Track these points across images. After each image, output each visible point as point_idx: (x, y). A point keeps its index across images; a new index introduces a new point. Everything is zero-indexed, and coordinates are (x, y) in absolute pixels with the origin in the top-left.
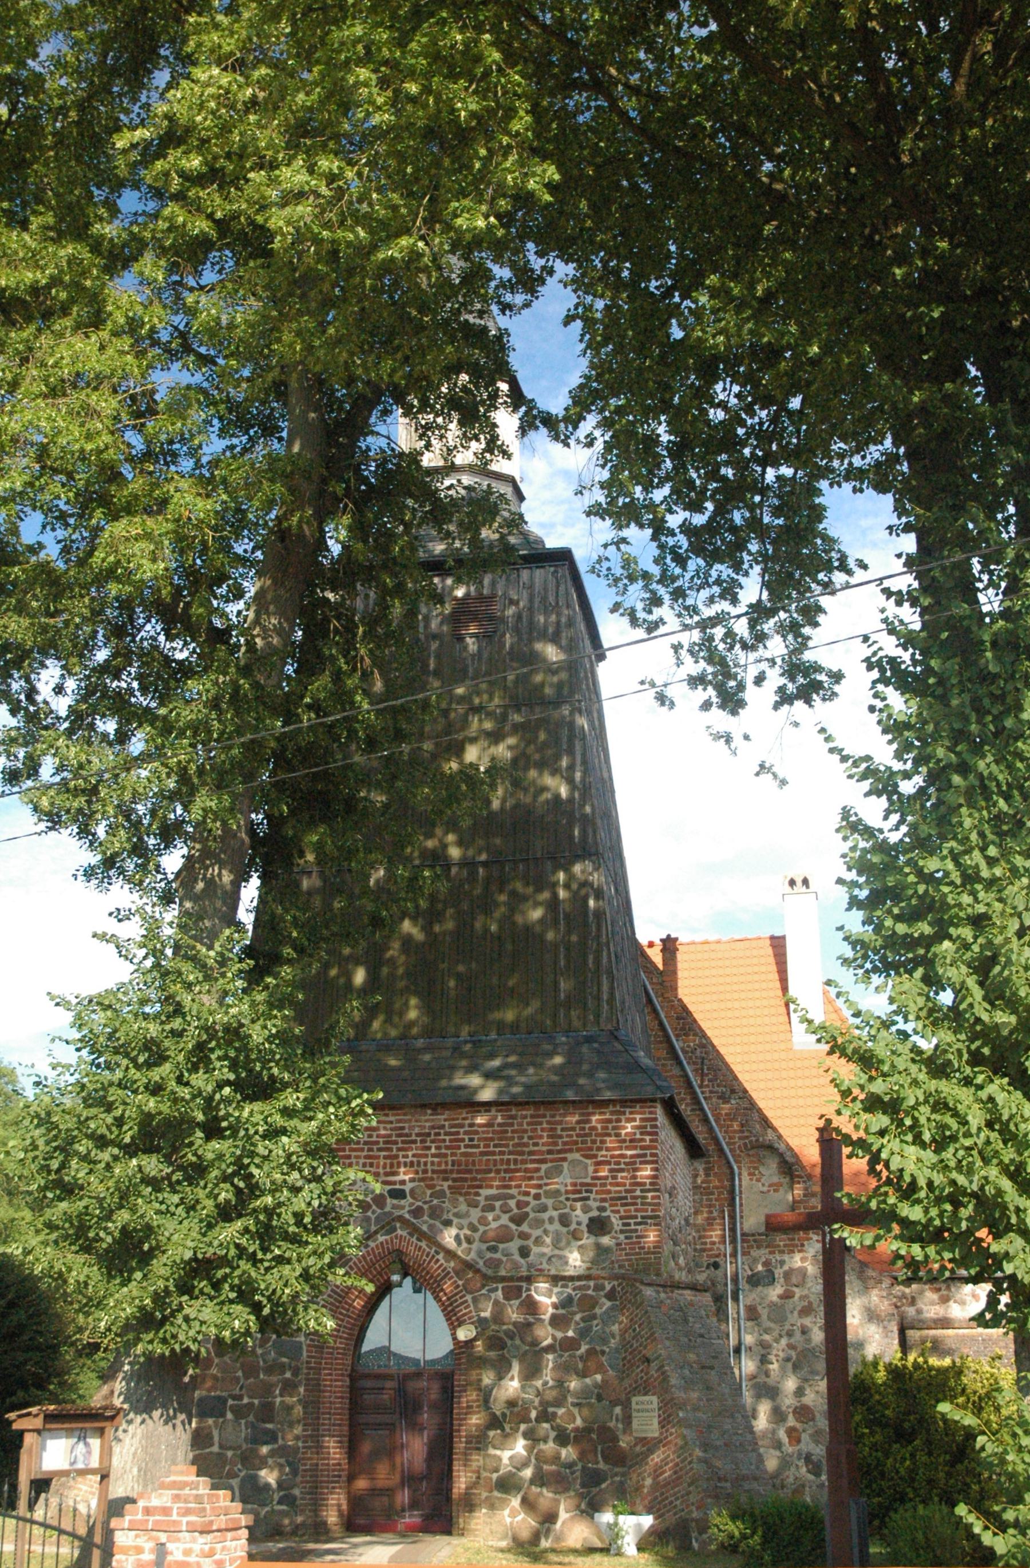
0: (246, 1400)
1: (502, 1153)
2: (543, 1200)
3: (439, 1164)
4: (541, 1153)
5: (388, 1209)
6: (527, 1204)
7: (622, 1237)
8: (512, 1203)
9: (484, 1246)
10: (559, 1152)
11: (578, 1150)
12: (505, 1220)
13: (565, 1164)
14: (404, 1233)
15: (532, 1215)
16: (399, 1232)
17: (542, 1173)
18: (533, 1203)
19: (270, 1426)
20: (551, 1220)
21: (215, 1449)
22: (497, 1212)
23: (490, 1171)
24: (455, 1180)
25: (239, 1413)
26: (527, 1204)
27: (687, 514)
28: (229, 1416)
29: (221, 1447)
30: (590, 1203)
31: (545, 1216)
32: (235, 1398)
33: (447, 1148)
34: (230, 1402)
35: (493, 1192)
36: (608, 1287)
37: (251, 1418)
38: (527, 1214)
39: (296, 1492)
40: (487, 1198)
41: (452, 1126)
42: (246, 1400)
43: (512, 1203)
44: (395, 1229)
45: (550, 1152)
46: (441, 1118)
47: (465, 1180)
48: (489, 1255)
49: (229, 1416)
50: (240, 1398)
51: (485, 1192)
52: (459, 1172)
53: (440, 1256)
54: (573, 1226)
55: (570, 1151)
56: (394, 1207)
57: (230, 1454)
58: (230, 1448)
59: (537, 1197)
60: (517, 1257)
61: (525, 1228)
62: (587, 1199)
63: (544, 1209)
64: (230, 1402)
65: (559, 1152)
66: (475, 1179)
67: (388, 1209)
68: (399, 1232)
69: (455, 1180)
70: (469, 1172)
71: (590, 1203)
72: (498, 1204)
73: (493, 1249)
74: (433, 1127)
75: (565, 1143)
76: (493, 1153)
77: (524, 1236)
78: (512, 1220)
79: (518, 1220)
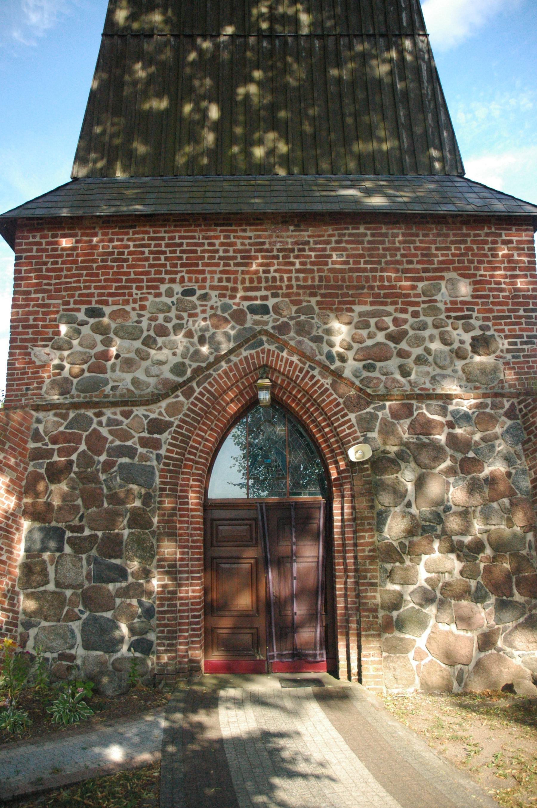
0: (87, 532)
1: (373, 270)
2: (422, 318)
3: (305, 279)
4: (417, 271)
5: (248, 324)
6: (405, 321)
7: (509, 356)
8: (388, 320)
9: (360, 365)
10: (435, 270)
11: (455, 269)
12: (380, 337)
13: (443, 283)
14: (272, 348)
15: (411, 332)
16: (266, 346)
17: (419, 291)
18: (411, 320)
19: (117, 561)
20: (432, 338)
21: (51, 587)
22: (373, 328)
23: (363, 288)
24: (323, 296)
25: (79, 546)
26: (405, 321)
27: (126, 324)
28: (67, 549)
29: (58, 584)
30: (472, 321)
31: (426, 333)
32: (73, 529)
33: (312, 263)
34: (68, 534)
35: (368, 308)
36: (507, 405)
37: (94, 552)
38: (406, 332)
39: (152, 636)
40: (361, 314)
41: (316, 243)
42: (87, 532)
43: (388, 320)
44: (261, 343)
45: (425, 270)
46: (305, 235)
47: (337, 296)
48: (365, 374)
49: (67, 549)
50: (81, 529)
51: (358, 309)
52: (327, 287)
53: (316, 372)
54: (456, 345)
55: (448, 270)
56: (256, 323)
57: (68, 593)
58: (68, 587)
59: (415, 315)
60: (398, 377)
61: (404, 345)
62: (470, 317)
63: (423, 327)
64: (68, 534)
65: (435, 270)
66: (347, 295)
67: (248, 324)
68: (266, 346)
69: (323, 296)
70: (340, 287)
71: (472, 321)
72: (373, 321)
73: (369, 368)
74: (296, 243)
75: (440, 262)
76: (365, 270)
77: (402, 354)
78: (390, 337)
79: (396, 338)
